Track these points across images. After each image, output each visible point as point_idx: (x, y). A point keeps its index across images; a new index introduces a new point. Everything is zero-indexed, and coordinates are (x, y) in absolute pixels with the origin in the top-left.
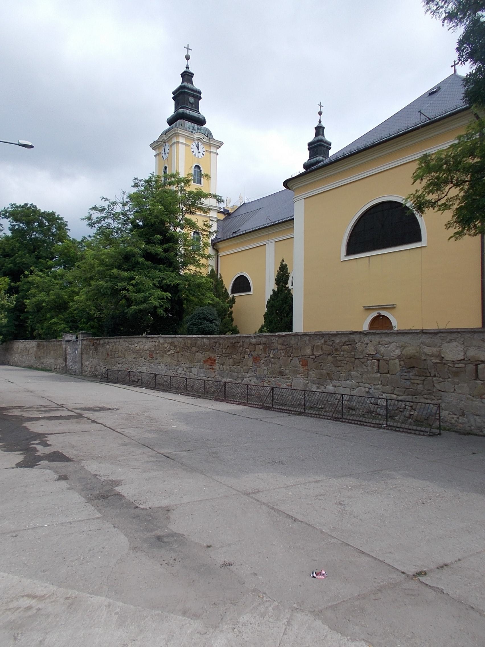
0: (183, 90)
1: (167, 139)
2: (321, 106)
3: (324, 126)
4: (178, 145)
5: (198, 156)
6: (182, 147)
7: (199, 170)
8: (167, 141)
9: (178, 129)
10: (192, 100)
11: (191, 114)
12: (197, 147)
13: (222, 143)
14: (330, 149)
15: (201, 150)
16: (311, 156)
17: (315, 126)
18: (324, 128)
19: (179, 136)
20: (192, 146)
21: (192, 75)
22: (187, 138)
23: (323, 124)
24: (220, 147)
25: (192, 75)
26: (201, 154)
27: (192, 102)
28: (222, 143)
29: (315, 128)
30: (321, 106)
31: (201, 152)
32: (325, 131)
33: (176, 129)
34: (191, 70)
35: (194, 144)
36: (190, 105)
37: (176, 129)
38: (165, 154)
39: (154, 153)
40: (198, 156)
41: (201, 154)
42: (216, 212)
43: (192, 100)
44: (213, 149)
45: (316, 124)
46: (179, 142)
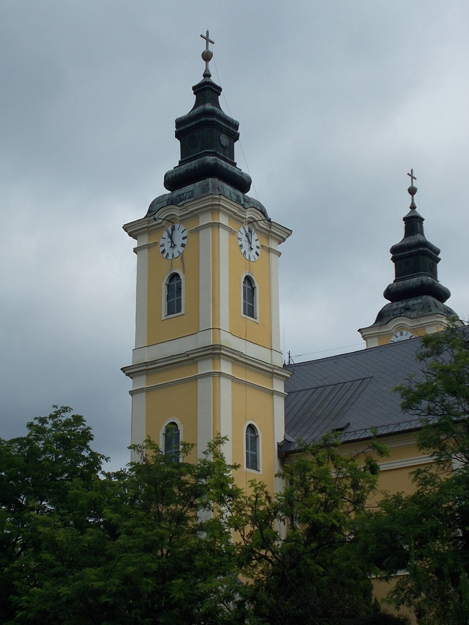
0: (211, 119)
1: (180, 216)
2: (413, 178)
3: (423, 216)
4: (216, 229)
5: (249, 257)
6: (224, 235)
7: (249, 287)
8: (180, 221)
9: (222, 197)
10: (224, 140)
11: (229, 169)
12: (247, 236)
13: (289, 232)
14: (438, 262)
15: (254, 244)
16: (399, 274)
17: (405, 215)
18: (423, 220)
19: (219, 211)
20: (240, 235)
21: (217, 90)
22: (233, 216)
23: (420, 211)
24: (284, 240)
25: (217, 90)
26: (254, 252)
27: (224, 144)
28: (289, 232)
29: (404, 219)
30: (413, 178)
31: (255, 249)
32: (424, 225)
33: (218, 197)
34: (214, 79)
35: (242, 230)
36: (222, 149)
37: (218, 197)
38: (173, 246)
39: (134, 243)
40: (249, 257)
41: (254, 252)
42: (231, 381)
43: (225, 140)
44: (273, 245)
45: (407, 211)
46: (219, 225)
